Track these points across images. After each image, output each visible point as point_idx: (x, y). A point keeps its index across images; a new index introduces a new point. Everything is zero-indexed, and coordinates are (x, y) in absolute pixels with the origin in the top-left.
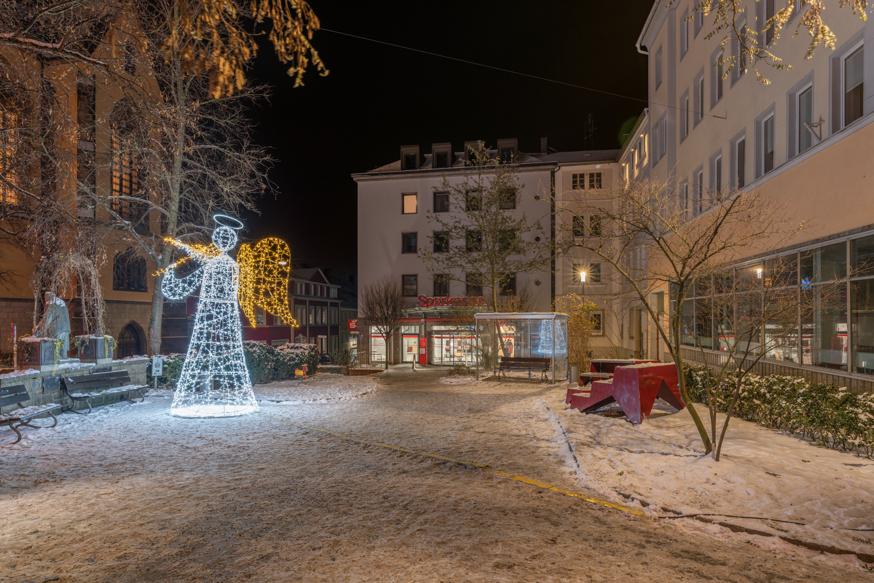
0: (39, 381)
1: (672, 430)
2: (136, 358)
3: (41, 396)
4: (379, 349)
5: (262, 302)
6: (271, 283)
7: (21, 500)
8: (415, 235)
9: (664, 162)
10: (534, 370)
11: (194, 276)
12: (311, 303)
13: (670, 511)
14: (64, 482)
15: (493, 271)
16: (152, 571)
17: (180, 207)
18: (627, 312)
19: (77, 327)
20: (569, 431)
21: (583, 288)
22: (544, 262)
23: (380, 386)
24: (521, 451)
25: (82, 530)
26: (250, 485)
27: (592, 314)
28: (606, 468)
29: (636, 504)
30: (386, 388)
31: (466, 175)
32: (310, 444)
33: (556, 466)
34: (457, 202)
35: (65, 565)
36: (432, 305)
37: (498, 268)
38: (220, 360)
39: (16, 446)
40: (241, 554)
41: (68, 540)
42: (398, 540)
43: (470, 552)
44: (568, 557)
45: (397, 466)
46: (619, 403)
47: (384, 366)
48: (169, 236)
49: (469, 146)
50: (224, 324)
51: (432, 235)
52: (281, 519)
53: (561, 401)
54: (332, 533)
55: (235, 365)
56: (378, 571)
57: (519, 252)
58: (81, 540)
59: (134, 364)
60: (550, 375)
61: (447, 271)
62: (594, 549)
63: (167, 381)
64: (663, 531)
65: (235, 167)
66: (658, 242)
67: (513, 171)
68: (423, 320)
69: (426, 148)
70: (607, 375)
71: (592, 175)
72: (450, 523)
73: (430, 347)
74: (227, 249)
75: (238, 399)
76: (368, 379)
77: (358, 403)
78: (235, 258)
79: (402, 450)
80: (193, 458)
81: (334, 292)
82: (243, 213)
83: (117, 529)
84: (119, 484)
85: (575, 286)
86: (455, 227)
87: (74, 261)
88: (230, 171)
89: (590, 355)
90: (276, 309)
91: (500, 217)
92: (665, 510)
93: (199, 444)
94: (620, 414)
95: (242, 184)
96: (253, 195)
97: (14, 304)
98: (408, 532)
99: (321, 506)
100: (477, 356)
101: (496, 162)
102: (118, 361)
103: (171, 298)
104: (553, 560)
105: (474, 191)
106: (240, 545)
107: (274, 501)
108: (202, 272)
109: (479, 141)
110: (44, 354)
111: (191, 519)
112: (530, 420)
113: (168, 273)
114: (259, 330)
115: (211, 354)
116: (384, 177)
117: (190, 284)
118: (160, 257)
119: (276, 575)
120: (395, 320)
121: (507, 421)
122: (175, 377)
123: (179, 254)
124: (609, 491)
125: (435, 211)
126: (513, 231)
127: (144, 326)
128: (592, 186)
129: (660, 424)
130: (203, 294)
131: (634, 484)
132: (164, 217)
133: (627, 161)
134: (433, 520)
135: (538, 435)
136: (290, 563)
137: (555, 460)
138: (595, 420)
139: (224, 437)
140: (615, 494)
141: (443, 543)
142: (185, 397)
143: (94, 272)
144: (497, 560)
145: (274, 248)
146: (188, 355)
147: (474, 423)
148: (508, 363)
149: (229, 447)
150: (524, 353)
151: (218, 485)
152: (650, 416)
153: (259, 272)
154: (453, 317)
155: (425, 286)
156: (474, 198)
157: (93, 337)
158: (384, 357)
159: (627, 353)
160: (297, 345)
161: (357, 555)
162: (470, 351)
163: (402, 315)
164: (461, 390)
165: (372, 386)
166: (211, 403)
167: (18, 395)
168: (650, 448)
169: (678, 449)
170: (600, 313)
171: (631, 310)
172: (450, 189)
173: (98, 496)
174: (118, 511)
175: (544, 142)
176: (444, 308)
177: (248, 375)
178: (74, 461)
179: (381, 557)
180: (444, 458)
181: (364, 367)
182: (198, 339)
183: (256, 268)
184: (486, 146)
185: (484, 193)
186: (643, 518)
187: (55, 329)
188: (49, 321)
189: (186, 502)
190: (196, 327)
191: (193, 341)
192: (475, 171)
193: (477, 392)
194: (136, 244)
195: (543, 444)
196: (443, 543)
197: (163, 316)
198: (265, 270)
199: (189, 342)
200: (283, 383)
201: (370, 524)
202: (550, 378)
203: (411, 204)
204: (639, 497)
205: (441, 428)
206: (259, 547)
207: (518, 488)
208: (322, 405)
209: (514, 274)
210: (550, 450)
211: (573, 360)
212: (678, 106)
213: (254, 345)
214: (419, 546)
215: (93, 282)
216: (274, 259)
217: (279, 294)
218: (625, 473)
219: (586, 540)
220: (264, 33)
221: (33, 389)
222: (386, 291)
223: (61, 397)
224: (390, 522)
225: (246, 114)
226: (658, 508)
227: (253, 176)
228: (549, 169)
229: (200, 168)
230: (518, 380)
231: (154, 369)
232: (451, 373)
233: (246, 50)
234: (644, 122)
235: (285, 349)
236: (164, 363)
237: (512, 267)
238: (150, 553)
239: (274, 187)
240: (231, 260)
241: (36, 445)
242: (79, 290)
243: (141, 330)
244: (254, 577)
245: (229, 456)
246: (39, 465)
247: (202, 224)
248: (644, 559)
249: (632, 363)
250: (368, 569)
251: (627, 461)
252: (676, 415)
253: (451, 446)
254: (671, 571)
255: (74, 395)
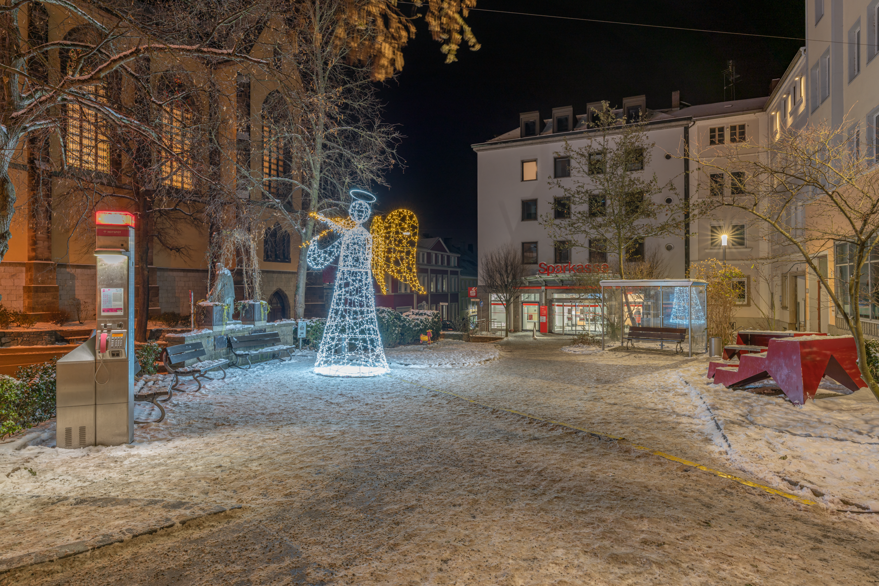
0: (212, 339)
1: (846, 413)
2: (285, 321)
3: (213, 352)
4: (499, 318)
5: (392, 271)
6: (401, 252)
7: (206, 439)
8: (535, 202)
9: (827, 108)
10: (667, 341)
11: (333, 247)
12: (433, 271)
13: (852, 504)
14: (237, 427)
15: (624, 233)
16: (314, 509)
17: (320, 184)
18: (778, 281)
19: (240, 294)
20: (714, 407)
21: (725, 252)
22: (677, 226)
23: (502, 353)
24: (659, 425)
25: (254, 468)
26: (389, 441)
27: (735, 280)
28: (764, 450)
29: (806, 493)
30: (509, 355)
31: (589, 138)
32: (440, 406)
33: (702, 445)
34: (578, 165)
35: (244, 497)
36: (552, 272)
37: (625, 232)
38: (355, 324)
39: (197, 394)
40: (388, 503)
41: (245, 475)
42: (536, 504)
43: (613, 524)
44: (726, 542)
45: (527, 433)
46: (775, 379)
47: (504, 333)
48: (311, 211)
49: (592, 108)
50: (358, 291)
51: (552, 201)
52: (420, 474)
53: (701, 375)
54: (470, 492)
55: (369, 329)
56: (519, 533)
57: (648, 216)
58: (255, 477)
59: (282, 326)
60: (686, 347)
61: (569, 237)
62: (757, 537)
63: (310, 343)
64: (844, 527)
65: (368, 144)
66: (830, 196)
67: (641, 130)
68: (543, 288)
69: (546, 114)
70: (759, 348)
71: (733, 128)
72: (589, 493)
73: (550, 315)
74: (361, 221)
75: (370, 360)
76: (489, 346)
77: (482, 369)
78: (368, 230)
79: (531, 417)
80: (338, 412)
81: (454, 261)
82: (375, 187)
83: (282, 470)
84: (280, 431)
85: (715, 251)
86: (578, 192)
87: (239, 236)
88: (363, 149)
89: (732, 326)
90: (405, 277)
91: (627, 179)
92: (845, 503)
93: (341, 400)
94: (776, 392)
95: (374, 161)
96: (383, 170)
97: (189, 274)
98: (546, 499)
99: (456, 466)
100: (603, 325)
101: (622, 121)
102: (271, 324)
103: (315, 267)
104: (709, 543)
105: (598, 154)
106: (387, 494)
107: (412, 457)
108: (340, 244)
109: (603, 102)
110: (216, 316)
111: (342, 467)
112: (666, 394)
113: (312, 244)
114: (388, 296)
115: (347, 318)
116: (504, 145)
117: (330, 254)
118: (304, 231)
119: (421, 526)
120: (515, 287)
121: (640, 394)
122: (316, 339)
123: (320, 227)
124: (770, 475)
125: (555, 177)
126: (641, 193)
127: (289, 293)
128: (733, 140)
129: (829, 405)
130: (341, 263)
131: (802, 471)
132: (308, 194)
133: (778, 108)
134: (570, 489)
135: (677, 410)
136: (434, 516)
137: (700, 438)
138: (744, 398)
139: (362, 396)
140: (778, 480)
141: (583, 513)
142: (327, 357)
143: (253, 245)
144: (643, 536)
145: (403, 219)
146: (329, 319)
147: (604, 393)
148: (638, 332)
149: (367, 404)
150: (653, 322)
151: (361, 438)
152: (813, 395)
153: (390, 242)
154: (575, 284)
155: (546, 254)
156: (598, 161)
157: (251, 302)
158: (504, 324)
159: (779, 324)
160: (421, 311)
161: (496, 516)
162: (594, 320)
163: (522, 283)
164: (587, 359)
165: (494, 353)
166: (348, 363)
167: (198, 351)
168: (818, 431)
169: (856, 435)
170: (745, 280)
171: (784, 276)
172: (572, 154)
173: (264, 440)
174: (281, 455)
175: (676, 96)
176: (566, 276)
177: (380, 339)
178: (242, 410)
179: (520, 519)
180: (575, 427)
181: (484, 334)
182: (338, 304)
183: (387, 238)
184: (611, 106)
185: (609, 155)
186: (816, 509)
187: (222, 297)
188: (219, 287)
189: (336, 451)
190: (336, 294)
191: (333, 306)
192: (599, 133)
193: (604, 362)
194: (284, 219)
195: (684, 420)
196: (583, 513)
197: (307, 284)
198: (395, 240)
199: (329, 308)
200: (409, 347)
201: (505, 486)
202: (686, 350)
203: (531, 171)
204: (809, 485)
205: (568, 400)
206: (403, 498)
207: (660, 463)
208: (447, 369)
209: (642, 238)
210: (693, 426)
211: (714, 332)
212: (845, 39)
213: (383, 311)
214: (558, 513)
215: (252, 254)
216: (403, 229)
217: (408, 263)
218: (789, 457)
219: (746, 526)
220: (421, 15)
221: (208, 346)
222: (506, 259)
223: (228, 353)
224: (526, 487)
225: (377, 95)
226: (836, 500)
227: (383, 152)
228: (681, 125)
229: (337, 149)
230: (649, 351)
231: (299, 331)
232: (574, 342)
233: (404, 34)
234: (800, 63)
235: (410, 315)
236: (307, 326)
237: (640, 231)
238: (311, 494)
239: (402, 161)
240: (365, 232)
241: (212, 393)
242: (240, 262)
243: (286, 296)
244: (403, 525)
245: (368, 413)
246: (217, 412)
247: (339, 199)
248: (822, 555)
249: (790, 336)
250: (509, 530)
251: (790, 444)
252: (850, 396)
253: (581, 416)
254: (859, 572)
255: (238, 352)
